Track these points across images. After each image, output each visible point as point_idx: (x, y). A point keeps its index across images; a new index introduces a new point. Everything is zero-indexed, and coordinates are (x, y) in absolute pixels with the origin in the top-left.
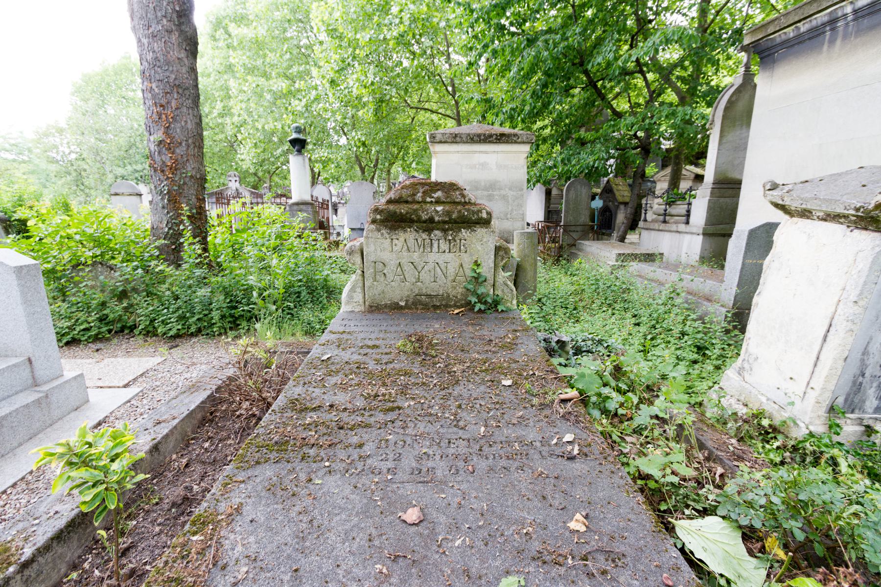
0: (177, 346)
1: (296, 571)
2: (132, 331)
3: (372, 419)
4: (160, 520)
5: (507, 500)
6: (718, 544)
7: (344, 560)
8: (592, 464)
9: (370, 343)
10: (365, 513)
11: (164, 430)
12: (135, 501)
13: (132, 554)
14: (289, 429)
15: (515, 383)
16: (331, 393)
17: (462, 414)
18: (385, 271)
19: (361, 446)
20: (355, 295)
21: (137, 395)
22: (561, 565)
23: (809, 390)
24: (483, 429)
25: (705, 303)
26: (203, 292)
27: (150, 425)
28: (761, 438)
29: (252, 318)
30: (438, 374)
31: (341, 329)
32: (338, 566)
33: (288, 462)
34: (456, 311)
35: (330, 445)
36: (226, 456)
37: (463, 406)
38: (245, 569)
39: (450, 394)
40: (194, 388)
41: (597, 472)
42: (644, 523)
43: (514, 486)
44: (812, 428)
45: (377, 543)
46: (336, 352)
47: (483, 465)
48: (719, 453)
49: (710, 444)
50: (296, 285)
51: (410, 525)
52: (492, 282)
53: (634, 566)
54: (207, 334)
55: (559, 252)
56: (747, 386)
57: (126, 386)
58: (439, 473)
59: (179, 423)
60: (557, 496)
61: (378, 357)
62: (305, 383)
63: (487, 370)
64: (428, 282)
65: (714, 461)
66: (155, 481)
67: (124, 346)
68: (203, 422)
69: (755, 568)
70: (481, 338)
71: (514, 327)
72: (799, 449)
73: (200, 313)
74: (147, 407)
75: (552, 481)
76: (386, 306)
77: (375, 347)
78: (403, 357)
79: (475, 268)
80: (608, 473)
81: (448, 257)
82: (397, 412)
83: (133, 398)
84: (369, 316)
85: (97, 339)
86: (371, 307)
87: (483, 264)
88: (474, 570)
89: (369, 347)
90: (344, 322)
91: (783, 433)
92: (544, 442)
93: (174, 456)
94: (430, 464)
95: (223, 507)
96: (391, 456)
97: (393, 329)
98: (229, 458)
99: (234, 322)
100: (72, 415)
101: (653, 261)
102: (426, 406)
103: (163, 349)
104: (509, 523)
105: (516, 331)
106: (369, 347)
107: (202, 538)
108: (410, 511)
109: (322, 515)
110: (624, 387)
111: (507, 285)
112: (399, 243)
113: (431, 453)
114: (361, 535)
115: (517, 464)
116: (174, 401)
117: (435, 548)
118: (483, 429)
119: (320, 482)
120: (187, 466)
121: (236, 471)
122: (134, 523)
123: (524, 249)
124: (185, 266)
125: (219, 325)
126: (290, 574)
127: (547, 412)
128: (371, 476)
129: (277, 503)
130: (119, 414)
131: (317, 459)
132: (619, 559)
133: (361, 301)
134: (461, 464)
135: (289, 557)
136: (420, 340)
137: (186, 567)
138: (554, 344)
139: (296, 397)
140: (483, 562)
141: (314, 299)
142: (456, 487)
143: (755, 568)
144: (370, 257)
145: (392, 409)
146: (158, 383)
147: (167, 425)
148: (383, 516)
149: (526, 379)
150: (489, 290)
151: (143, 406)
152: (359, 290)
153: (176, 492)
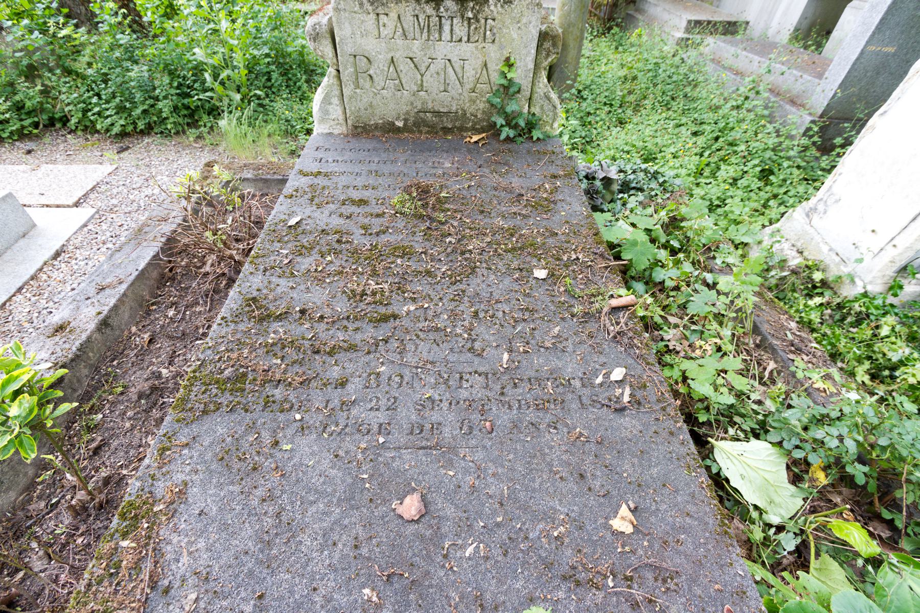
0: (128, 148)
1: (261, 597)
2: (64, 125)
3: (359, 336)
4: (130, 413)
5: (534, 481)
6: (760, 472)
7: (322, 579)
8: (645, 418)
9: (356, 195)
10: (349, 500)
11: (110, 300)
12: (96, 389)
13: (106, 454)
14: (246, 352)
15: (551, 275)
16: (302, 287)
17: (480, 329)
18: (371, 72)
19: (343, 384)
20: (330, 108)
21: (92, 217)
22: (597, 588)
23: (890, 246)
24: (506, 356)
25: (788, 107)
26: (137, 72)
27: (92, 291)
28: (806, 292)
29: (215, 112)
30: (448, 255)
31: (314, 167)
32: (315, 589)
33: (246, 411)
34: (475, 138)
35: (301, 383)
36: (197, 328)
37: (481, 315)
38: (193, 596)
39: (463, 291)
40: (139, 233)
41: (651, 433)
42: (707, 519)
43: (544, 455)
44: (869, 288)
45: (364, 551)
46: (308, 212)
47: (503, 417)
48: (775, 342)
49: (765, 328)
50: (262, 62)
51: (408, 521)
52: (528, 94)
53: (690, 590)
54: (162, 133)
55: (611, 13)
56: (812, 231)
57: (77, 204)
58: (447, 432)
59: (128, 289)
60: (598, 473)
61: (366, 221)
62: (265, 270)
63: (514, 249)
64: (435, 91)
65: (765, 349)
66: (115, 363)
67: (61, 147)
68: (162, 281)
69: (792, 496)
70: (508, 190)
71: (553, 170)
72: (844, 308)
73: (143, 103)
74: (108, 234)
75: (593, 447)
76: (376, 126)
77: (362, 202)
78: (400, 223)
79: (506, 70)
80: (665, 434)
81: (466, 49)
82: (392, 323)
83: (89, 221)
84: (355, 143)
85: (21, 135)
86: (356, 127)
87: (518, 64)
88: (488, 596)
89: (353, 202)
90: (320, 154)
91: (832, 288)
92: (586, 382)
93: (134, 329)
94: (435, 417)
95: (161, 488)
96: (383, 402)
97: (386, 169)
98: (201, 331)
99: (191, 116)
100: (22, 242)
101: (733, 33)
102: (431, 313)
103: (110, 153)
104: (535, 519)
105: (555, 177)
106: (353, 202)
107: (134, 545)
108: (408, 500)
109: (292, 503)
110: (676, 244)
111: (549, 98)
112: (390, 22)
113: (437, 397)
114: (344, 537)
115: (549, 418)
116: (118, 255)
117: (439, 559)
118: (506, 356)
119: (289, 447)
120: (151, 341)
121: (176, 426)
122: (100, 416)
123: (569, 14)
124: (104, 28)
125: (172, 120)
126: (252, 602)
127: (592, 327)
128: (358, 436)
129: (232, 483)
130: (77, 242)
131: (286, 407)
132: (672, 579)
133: (341, 118)
134: (475, 417)
135: (251, 573)
136: (424, 191)
137: (116, 592)
138: (598, 183)
139: (255, 294)
140: (501, 582)
141: (291, 85)
142: (468, 458)
143: (792, 496)
144: (346, 48)
145: (385, 319)
146: (115, 201)
147: (113, 292)
148: (373, 506)
149: (566, 266)
150: (522, 107)
151: (104, 232)
152: (335, 101)
153: (139, 381)
